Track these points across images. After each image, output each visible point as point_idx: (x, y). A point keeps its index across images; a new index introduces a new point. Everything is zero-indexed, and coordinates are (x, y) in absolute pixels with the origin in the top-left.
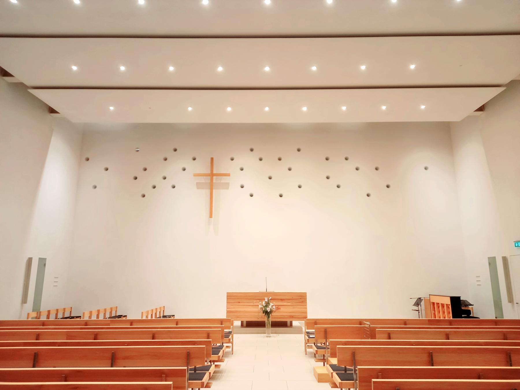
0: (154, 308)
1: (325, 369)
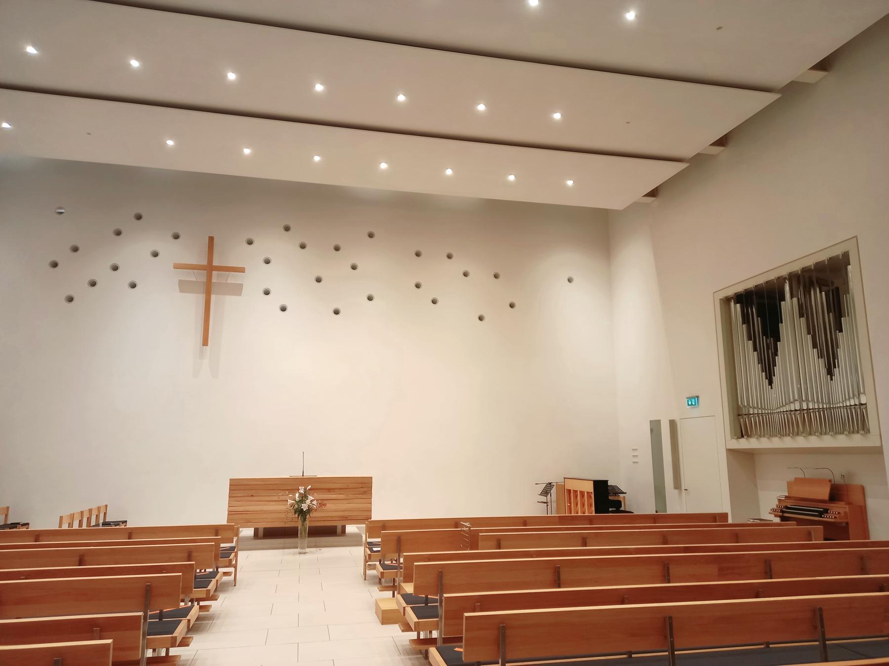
1: (389, 601)
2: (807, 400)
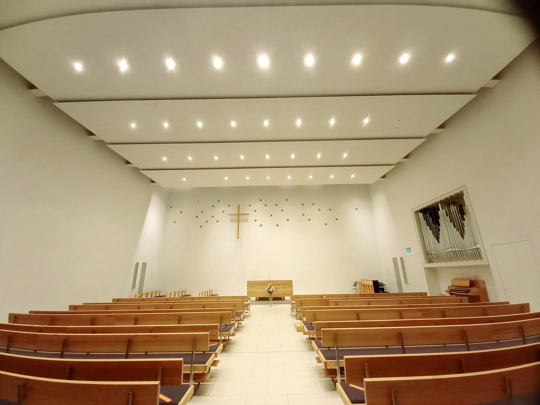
0: (209, 290)
1: (300, 323)
2: (454, 247)
